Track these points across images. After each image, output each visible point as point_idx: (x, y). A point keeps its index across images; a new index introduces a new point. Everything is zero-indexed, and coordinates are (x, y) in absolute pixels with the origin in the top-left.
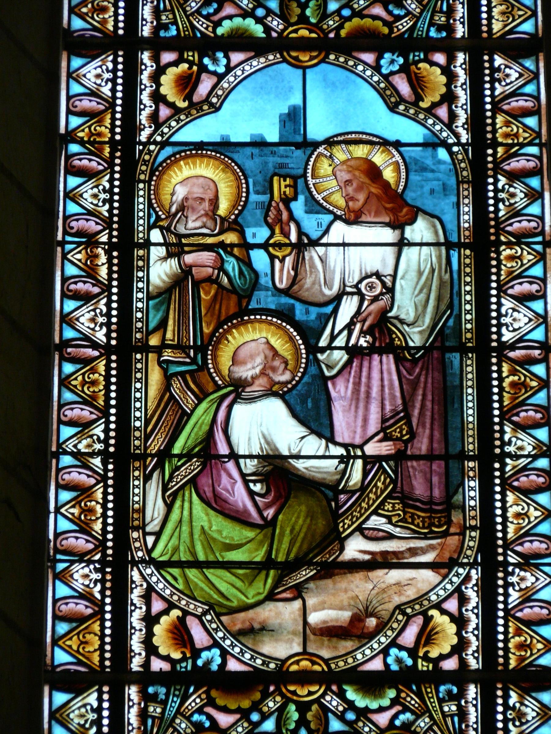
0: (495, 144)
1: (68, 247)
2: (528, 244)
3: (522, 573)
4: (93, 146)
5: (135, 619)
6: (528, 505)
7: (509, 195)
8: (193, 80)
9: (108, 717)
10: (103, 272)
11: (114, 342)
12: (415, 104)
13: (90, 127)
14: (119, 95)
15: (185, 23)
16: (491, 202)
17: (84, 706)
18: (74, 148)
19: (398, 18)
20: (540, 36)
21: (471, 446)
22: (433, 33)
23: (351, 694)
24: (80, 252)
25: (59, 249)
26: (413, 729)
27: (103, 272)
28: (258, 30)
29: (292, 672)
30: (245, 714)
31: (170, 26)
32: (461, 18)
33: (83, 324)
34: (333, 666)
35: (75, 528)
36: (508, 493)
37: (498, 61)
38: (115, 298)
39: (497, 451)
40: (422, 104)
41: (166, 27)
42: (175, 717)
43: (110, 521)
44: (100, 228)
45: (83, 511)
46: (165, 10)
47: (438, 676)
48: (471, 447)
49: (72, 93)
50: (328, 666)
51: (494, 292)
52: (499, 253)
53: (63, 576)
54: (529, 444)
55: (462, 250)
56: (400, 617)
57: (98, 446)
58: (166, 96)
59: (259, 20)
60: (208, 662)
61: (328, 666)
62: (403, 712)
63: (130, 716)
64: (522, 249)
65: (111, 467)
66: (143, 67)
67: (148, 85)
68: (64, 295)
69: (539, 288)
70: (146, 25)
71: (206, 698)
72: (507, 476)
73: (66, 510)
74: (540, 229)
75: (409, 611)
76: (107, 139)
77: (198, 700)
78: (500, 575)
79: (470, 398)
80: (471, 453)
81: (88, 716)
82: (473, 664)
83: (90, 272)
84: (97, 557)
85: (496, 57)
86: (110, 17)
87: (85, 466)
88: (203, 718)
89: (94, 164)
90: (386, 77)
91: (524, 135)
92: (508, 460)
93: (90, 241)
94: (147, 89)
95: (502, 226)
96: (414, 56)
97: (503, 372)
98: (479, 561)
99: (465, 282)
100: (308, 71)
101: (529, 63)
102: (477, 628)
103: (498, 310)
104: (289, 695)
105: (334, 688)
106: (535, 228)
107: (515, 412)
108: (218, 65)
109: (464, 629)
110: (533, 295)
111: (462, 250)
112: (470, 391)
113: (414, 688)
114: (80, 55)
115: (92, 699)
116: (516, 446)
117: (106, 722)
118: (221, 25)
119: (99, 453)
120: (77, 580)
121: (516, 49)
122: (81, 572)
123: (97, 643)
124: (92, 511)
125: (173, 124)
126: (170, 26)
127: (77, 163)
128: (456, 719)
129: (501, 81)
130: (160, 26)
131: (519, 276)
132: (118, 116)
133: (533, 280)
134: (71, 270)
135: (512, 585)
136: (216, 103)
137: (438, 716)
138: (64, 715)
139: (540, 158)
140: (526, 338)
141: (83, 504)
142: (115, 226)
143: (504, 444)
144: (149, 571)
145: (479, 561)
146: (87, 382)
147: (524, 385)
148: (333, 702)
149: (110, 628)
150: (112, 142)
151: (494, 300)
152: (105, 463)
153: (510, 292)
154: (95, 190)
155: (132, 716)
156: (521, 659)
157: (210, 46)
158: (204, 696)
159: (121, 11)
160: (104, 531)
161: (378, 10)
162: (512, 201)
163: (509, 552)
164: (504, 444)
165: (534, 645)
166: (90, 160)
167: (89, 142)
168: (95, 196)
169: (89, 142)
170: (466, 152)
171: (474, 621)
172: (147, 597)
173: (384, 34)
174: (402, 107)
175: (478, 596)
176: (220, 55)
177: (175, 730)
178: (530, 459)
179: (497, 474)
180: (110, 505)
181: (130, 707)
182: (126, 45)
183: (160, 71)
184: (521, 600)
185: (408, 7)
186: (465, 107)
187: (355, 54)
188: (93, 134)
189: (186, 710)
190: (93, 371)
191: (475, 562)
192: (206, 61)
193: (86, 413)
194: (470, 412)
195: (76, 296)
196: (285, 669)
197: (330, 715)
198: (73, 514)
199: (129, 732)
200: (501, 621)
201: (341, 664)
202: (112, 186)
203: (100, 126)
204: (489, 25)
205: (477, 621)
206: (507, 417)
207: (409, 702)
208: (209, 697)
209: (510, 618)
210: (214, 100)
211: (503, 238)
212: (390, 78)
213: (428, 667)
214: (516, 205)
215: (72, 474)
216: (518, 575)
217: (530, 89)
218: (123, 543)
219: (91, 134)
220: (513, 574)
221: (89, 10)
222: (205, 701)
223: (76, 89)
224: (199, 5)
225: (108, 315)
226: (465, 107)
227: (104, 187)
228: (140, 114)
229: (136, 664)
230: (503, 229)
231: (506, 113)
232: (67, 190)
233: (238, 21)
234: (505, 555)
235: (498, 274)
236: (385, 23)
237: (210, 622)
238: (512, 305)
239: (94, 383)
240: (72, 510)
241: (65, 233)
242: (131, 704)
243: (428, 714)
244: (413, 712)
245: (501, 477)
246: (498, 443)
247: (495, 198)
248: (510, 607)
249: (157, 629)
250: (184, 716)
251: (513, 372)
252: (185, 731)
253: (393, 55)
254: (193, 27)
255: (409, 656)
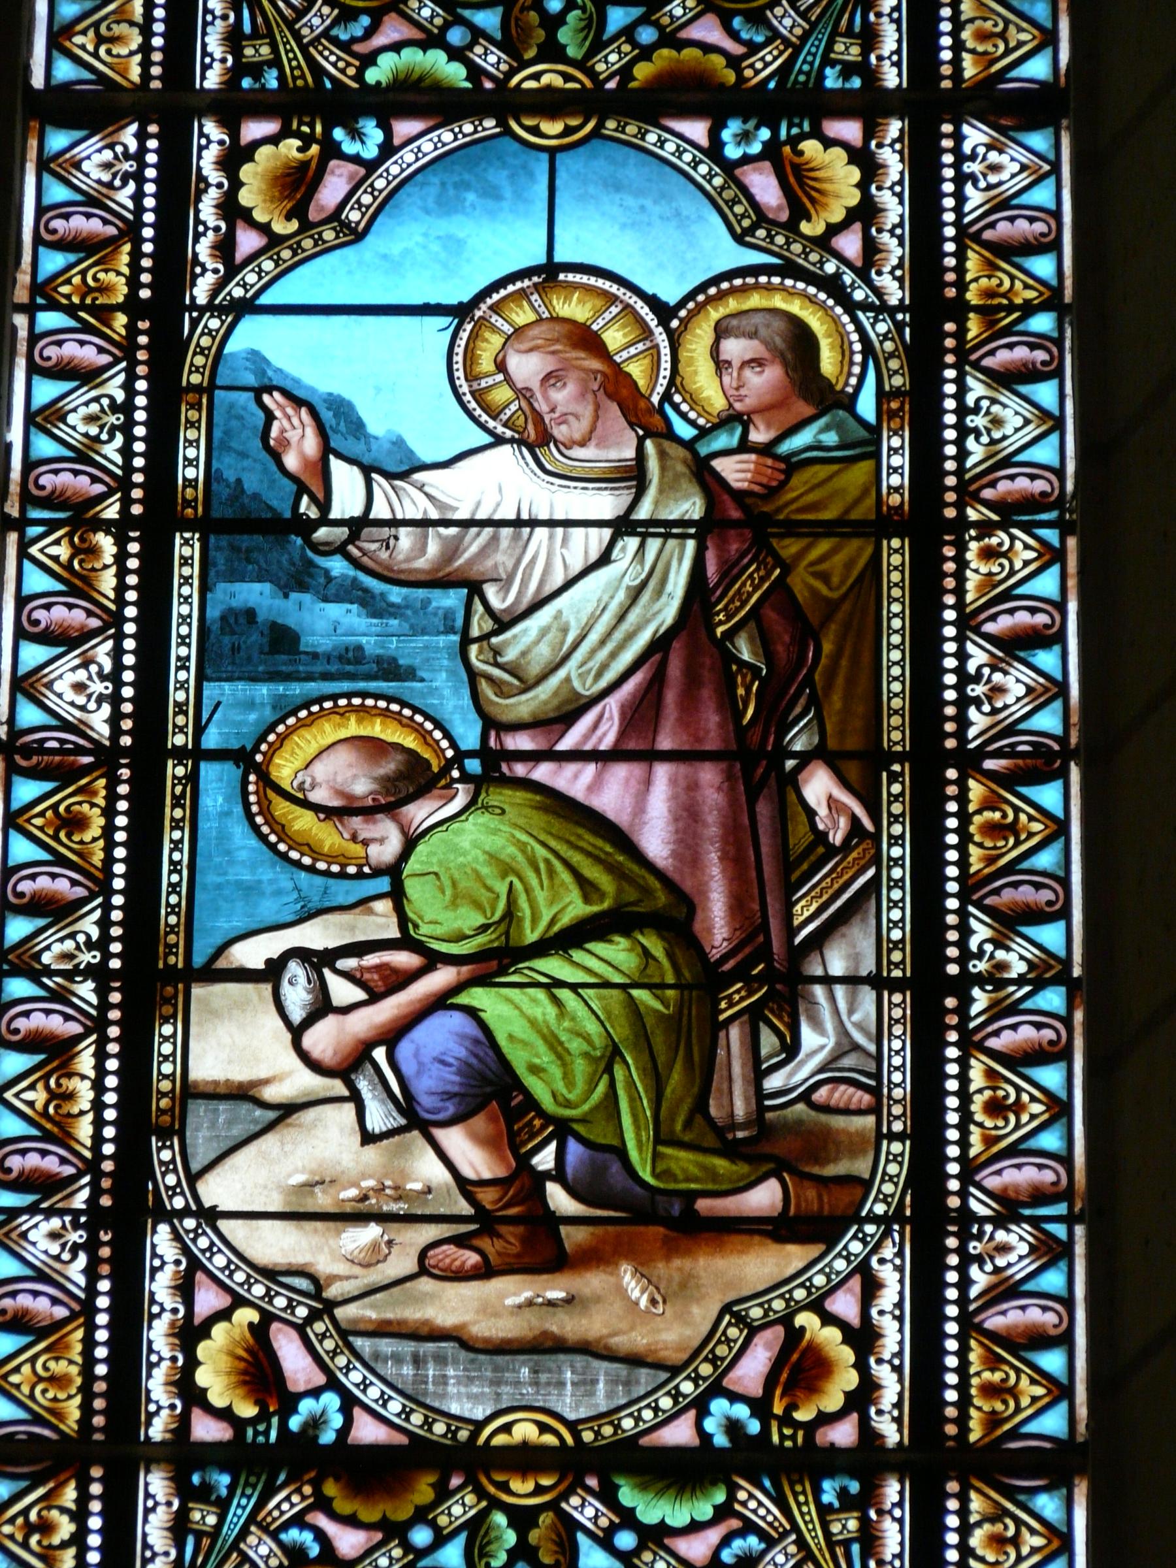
0: (959, 311)
1: (33, 531)
2: (1027, 528)
3: (1001, 1236)
4: (91, 314)
5: (894, 209)
6: (1018, 1371)
7: (991, 421)
8: (311, 173)
9: (100, 1514)
10: (107, 582)
11: (126, 741)
12: (791, 226)
13: (83, 273)
14: (149, 202)
15: (296, 58)
16: (950, 434)
17: (96, 400)
18: (48, 320)
19: (298, 1521)
20: (1072, 764)
21: (896, 734)
22: (832, 80)
23: (627, 1496)
24: (57, 542)
25: (12, 538)
26: (336, 11)
27: (107, 582)
28: (456, 73)
29: (496, 1447)
30: (670, 39)
31: (836, 1504)
32: (894, 1355)
33: (60, 696)
34: (588, 1436)
35: (60, 587)
36: (973, 1495)
37: (975, 136)
38: (148, 248)
39: (953, 969)
40: (805, 228)
41: (256, 70)
42: (244, 1533)
43: (121, 821)
44: (105, 359)
45: (52, 1095)
46: (255, 34)
47: (814, 1462)
48: (896, 736)
49: (27, 590)
50: (576, 1435)
51: (951, 497)
52: (962, 547)
53: (32, 685)
54: (1017, 413)
55: (886, 994)
56: (733, 1332)
57: (89, 958)
58: (205, 1390)
59: (456, 54)
60: (316, 1423)
61: (576, 1435)
62: (742, 1533)
63: (148, 1529)
64: (1013, 538)
65: (115, 998)
66: (198, 270)
67: (168, 1306)
68: (38, 241)
69: (1052, 897)
70: (212, 23)
71: (312, 1495)
72: (972, 1025)
73: (41, 551)
74: (1052, 236)
75: (756, 1313)
76: (121, 299)
77: (759, 65)
78: (952, 1242)
79: (897, 593)
80: (899, 748)
81: (105, 419)
82: (891, 1434)
83: (77, 585)
84: (112, 512)
85: (966, 129)
86: (95, 840)
87: (60, 996)
88: (307, 1537)
89: (88, 354)
90: (729, 168)
91: (1024, 295)
92: (976, 992)
93: (79, 517)
94: (212, 146)
95: (977, 1038)
96: (266, 1433)
97: (970, 801)
98: (908, 1213)
99: (889, 900)
100: (560, 157)
101: (1039, 140)
102: (900, 265)
103: (962, 944)
104: (492, 1490)
105: (592, 1482)
106: (1050, 903)
107: (990, 1029)
108: (323, 1413)
109: (872, 1353)
110: (1042, 911)
111: (886, 994)
112: (896, 671)
113: (767, 1483)
114: (64, 123)
115: (128, 137)
116: (993, 1244)
117: (94, 1540)
118: (374, 63)
119: (90, 972)
120: (34, 1244)
121: (1010, 110)
122: (98, 158)
123: (136, 41)
124: (70, 1096)
125: (268, 265)
126: (836, 1504)
127: (52, 352)
128: (247, 28)
129: (982, 703)
130: (864, 1502)
131: (1006, 596)
132: (113, 1048)
133: (1037, 604)
134: (37, 582)
135: (973, 178)
136: (358, 223)
137: (815, 1539)
138: (14, 1235)
139: (1067, 1021)
140: (1022, 726)
141: (52, 1082)
142: (142, 355)
143: (966, 956)
144: (190, 1223)
145: (908, 1213)
146: (41, 1379)
147: (1014, 828)
148: (586, 1511)
149: (99, 1531)
150: (132, 306)
151: (950, 647)
152: (102, 992)
153: (989, 628)
154: (81, 675)
155: (154, 1529)
156: (993, 1420)
157: (348, 105)
158: (307, 1490)
159: (110, 1098)
160: (98, 1139)
161: (348, 1542)
162: (997, 435)
163: (971, 909)
164: (966, 956)
165: (1016, 554)
166: (54, 876)
167: (83, 307)
168: (79, 687)
169: (83, 307)
170: (900, 326)
171: (893, 1337)
172: (185, 1289)
173: (337, 1479)
174: (761, 233)
175: (902, 160)
176: (721, 1440)
177: (245, 1558)
178: (1027, 989)
179: (949, 343)
180: (122, 805)
181: (147, 1511)
182: (170, 106)
183: (235, 157)
184: (987, 207)
185: (775, 23)
186: (898, 231)
187: (403, 1440)
188: (91, 290)
189: (269, 1519)
190: (57, 1350)
191: (898, 1216)
192: (338, 134)
193: (62, 885)
194: (896, 639)
195: (45, 638)
196: (481, 1440)
197: (581, 1537)
198: (55, 559)
199: (897, 8)
200: (952, 1345)
201: (607, 1430)
202: (118, 667)
203: (106, 271)
204: (956, 62)
205: (899, 210)
206: (975, 897)
207: (754, 1511)
208: (739, 72)
209: (967, 368)
210: (355, 216)
211: (972, 515)
212: (738, 172)
213: (793, 1438)
214: (1010, 1272)
215: (66, 346)
216: (988, 413)
217: (1042, 195)
218: (134, 1164)
219: (86, 290)
220: (979, 1237)
221: (77, 289)
222: (311, 1500)
223: (58, 193)
224: (328, 22)
225: (115, 677)
226: (898, 231)
227: (88, 936)
228: (145, 1521)
229: (158, 1430)
230: (977, 238)
231: (993, 1336)
232: (20, 673)
233: (412, 56)
234: (963, 1194)
235: (960, 591)
236: (734, 62)
237: (322, 1337)
238: (985, 139)
239: (57, 1381)
240: (29, 1096)
241: (27, 499)
242: (148, 1554)
243: (794, 1537)
244: (335, 41)
245: (961, 1028)
246: (952, 952)
247: (960, 427)
248: (967, 220)
249: (246, 172)
250: (265, 1529)
251: (993, 1362)
252: (266, 1563)
253: (745, 122)
254: (318, 71)
255: (753, 1415)
